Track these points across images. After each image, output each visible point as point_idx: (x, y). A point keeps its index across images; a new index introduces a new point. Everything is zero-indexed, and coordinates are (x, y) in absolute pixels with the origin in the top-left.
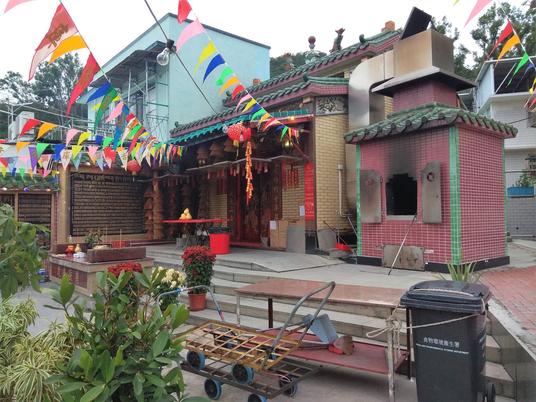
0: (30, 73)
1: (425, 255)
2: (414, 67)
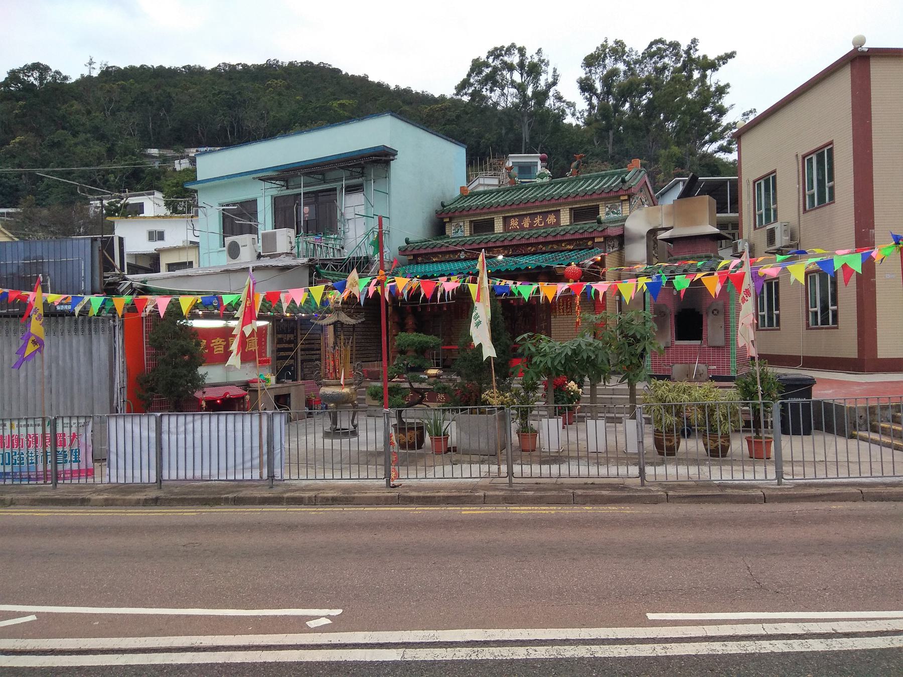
0: (228, 177)
1: (709, 371)
2: (694, 223)
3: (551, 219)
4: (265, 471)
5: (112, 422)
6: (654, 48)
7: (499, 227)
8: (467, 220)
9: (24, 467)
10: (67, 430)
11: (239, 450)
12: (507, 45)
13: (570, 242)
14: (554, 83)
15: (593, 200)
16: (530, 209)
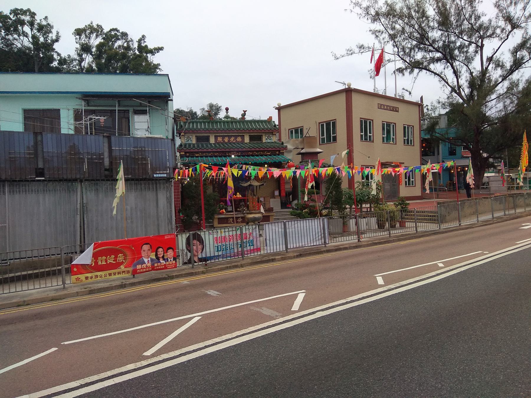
0: (39, 92)
3: (239, 139)
4: (323, 241)
5: (179, 237)
6: (113, 33)
7: (212, 140)
8: (194, 136)
9: (228, 251)
10: (247, 232)
11: (314, 233)
12: (25, 8)
13: (268, 151)
14: (57, 40)
15: (260, 133)
16: (229, 133)
